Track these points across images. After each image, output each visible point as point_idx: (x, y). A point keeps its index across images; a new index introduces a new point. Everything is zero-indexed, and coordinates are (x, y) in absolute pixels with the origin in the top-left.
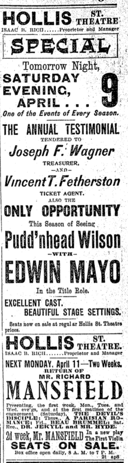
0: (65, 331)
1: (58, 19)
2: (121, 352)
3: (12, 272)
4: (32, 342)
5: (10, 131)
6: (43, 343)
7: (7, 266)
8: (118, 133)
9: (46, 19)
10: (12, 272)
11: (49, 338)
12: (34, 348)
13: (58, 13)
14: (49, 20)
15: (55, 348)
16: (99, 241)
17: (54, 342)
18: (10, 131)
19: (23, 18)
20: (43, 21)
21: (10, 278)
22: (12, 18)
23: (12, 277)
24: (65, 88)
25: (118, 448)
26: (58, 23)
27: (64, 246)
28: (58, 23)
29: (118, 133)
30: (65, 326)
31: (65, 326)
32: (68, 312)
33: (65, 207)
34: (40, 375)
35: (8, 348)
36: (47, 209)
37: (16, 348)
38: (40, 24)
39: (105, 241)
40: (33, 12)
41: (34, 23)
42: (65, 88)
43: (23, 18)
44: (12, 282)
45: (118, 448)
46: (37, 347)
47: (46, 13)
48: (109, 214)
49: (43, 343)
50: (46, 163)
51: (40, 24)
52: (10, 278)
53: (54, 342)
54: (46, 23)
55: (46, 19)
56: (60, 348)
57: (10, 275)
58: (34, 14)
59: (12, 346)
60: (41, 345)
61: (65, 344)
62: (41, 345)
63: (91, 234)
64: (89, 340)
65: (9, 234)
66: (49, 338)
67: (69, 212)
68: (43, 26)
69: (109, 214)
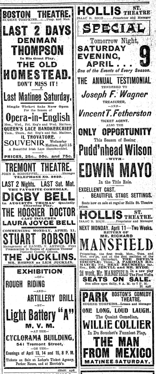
0: (117, 207)
1: (112, 11)
3: (83, 170)
5: (47, 168)
6: (103, 215)
7: (80, 166)
9: (105, 11)
10: (83, 170)
11: (106, 212)
12: (97, 218)
13: (112, 8)
14: (107, 12)
16: (138, 151)
17: (110, 214)
18: (47, 168)
19: (90, 11)
20: (103, 13)
21: (82, 174)
22: (83, 11)
23: (84, 173)
26: (112, 14)
27: (36, 318)
28: (112, 14)
30: (117, 204)
31: (117, 204)
34: (101, 235)
35: (79, 14)
36: (106, 131)
37: (86, 218)
38: (101, 14)
39: (142, 150)
41: (97, 14)
43: (90, 11)
44: (83, 176)
46: (99, 218)
49: (103, 215)
50: (105, 102)
51: (101, 14)
52: (82, 174)
53: (110, 214)
54: (105, 14)
55: (105, 11)
57: (82, 172)
58: (97, 8)
59: (83, 217)
64: (132, 213)
66: (106, 212)
68: (103, 16)
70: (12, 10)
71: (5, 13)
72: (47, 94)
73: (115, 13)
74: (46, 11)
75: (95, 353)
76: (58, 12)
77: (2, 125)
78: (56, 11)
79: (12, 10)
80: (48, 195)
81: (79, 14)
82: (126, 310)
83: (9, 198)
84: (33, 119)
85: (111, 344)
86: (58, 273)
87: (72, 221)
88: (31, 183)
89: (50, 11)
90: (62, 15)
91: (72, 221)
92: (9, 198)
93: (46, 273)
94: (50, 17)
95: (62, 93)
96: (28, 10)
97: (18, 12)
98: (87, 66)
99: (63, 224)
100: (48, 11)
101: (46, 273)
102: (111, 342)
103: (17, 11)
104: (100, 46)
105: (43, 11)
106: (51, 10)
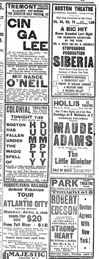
2: (30, 224)
3: (67, 200)
4: (63, 103)
6: (67, 103)
8: (20, 158)
9: (70, 104)
10: (67, 200)
11: (89, 162)
15: (72, 106)
19: (61, 103)
20: (68, 104)
24: (75, 28)
25: (81, 159)
28: (74, 106)
29: (20, 158)
32: (65, 48)
33: (59, 10)
38: (67, 105)
40: (28, 20)
41: (65, 105)
42: (75, 28)
43: (61, 103)
45: (81, 159)
47: (70, 101)
48: (42, 206)
51: (67, 105)
53: (72, 103)
54: (16, 136)
55: (70, 104)
56: (74, 106)
60: (66, 104)
61: (76, 104)
62: (66, 104)
63: (85, 222)
65: (81, 206)
66: (89, 162)
67: (68, 9)
68: (69, 106)
69: (42, 206)
70: (60, 6)
71: (56, 7)
72: (31, 217)
73: (76, 105)
74: (79, 7)
75: (57, 8)
76: (87, 8)
77: (94, 108)
78: (86, 7)
79: (60, 6)
80: (68, 28)
81: (55, 105)
82: (32, 63)
83: (73, 28)
84: (17, 141)
85: (92, 10)
86: (23, 126)
87: (15, 135)
88: (87, 206)
89: (82, 7)
90: (89, 10)
91: (15, 135)
92: (73, 28)
93: (17, 126)
94: (75, 66)
95: (86, 238)
96: (70, 6)
97: (64, 7)
98: (23, 213)
99: (14, 147)
100: (81, 7)
101: (17, 126)
102: (93, 9)
103: (64, 7)
104: (29, 194)
105: (78, 7)
106: (83, 6)
